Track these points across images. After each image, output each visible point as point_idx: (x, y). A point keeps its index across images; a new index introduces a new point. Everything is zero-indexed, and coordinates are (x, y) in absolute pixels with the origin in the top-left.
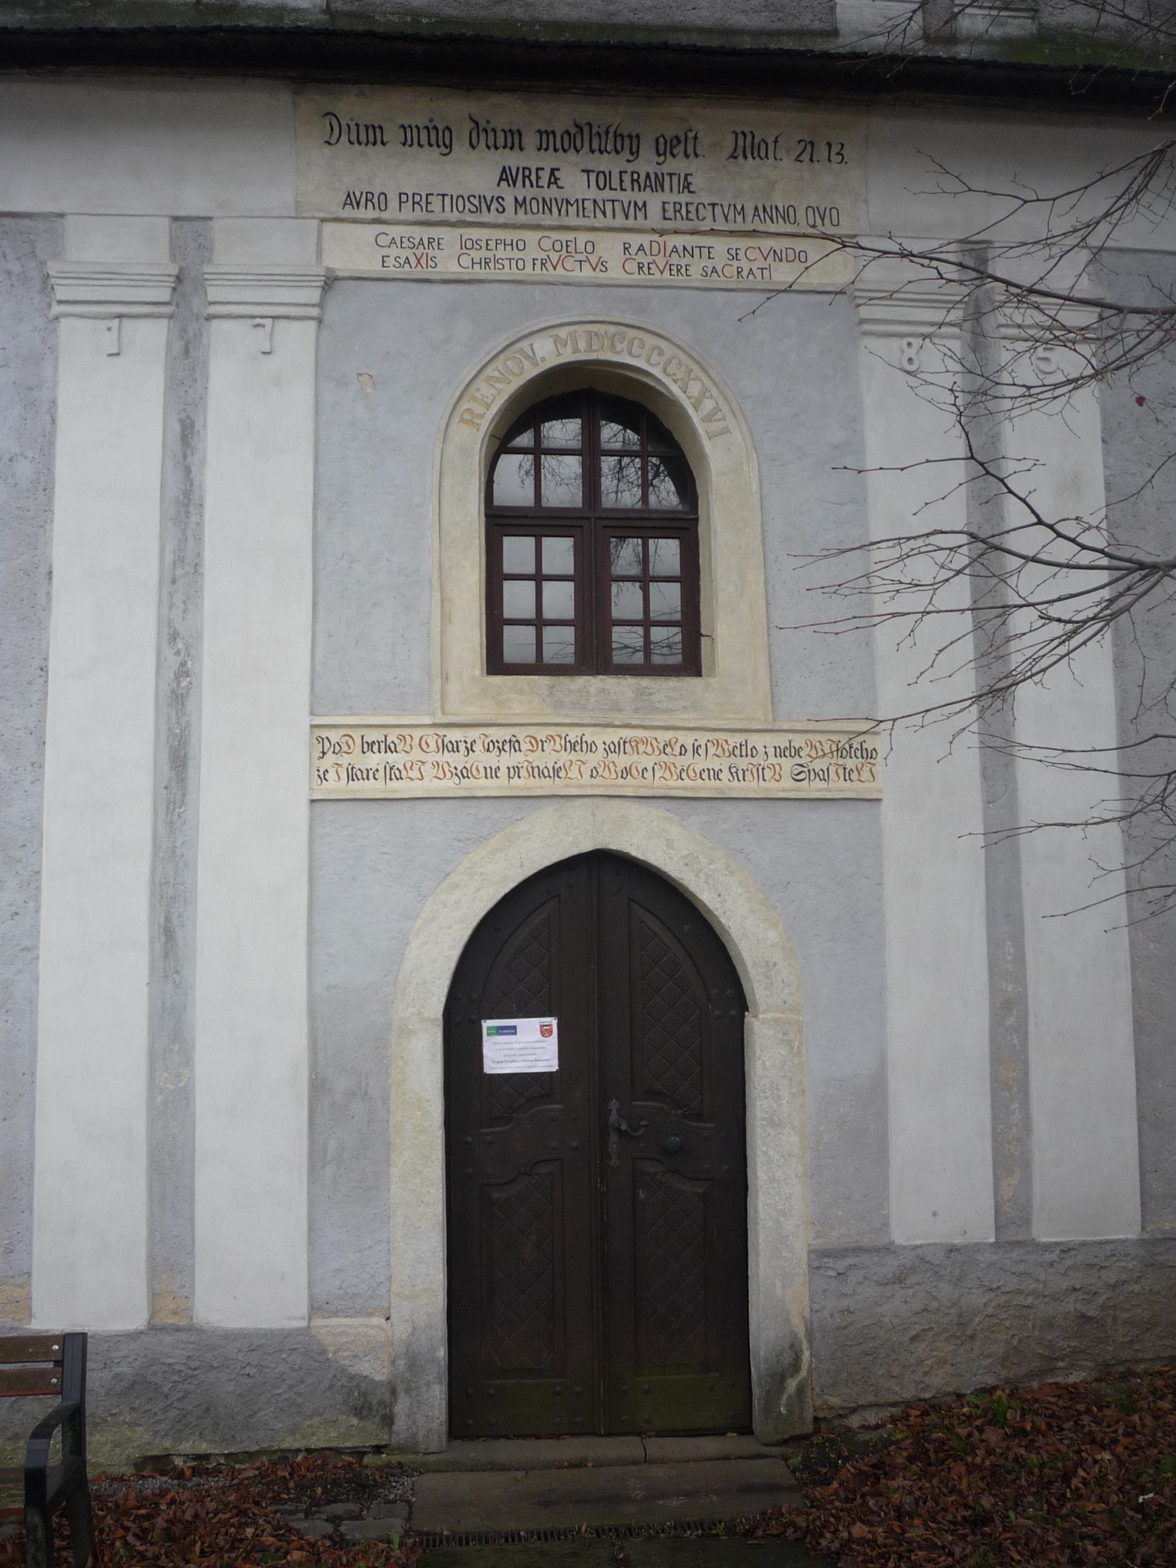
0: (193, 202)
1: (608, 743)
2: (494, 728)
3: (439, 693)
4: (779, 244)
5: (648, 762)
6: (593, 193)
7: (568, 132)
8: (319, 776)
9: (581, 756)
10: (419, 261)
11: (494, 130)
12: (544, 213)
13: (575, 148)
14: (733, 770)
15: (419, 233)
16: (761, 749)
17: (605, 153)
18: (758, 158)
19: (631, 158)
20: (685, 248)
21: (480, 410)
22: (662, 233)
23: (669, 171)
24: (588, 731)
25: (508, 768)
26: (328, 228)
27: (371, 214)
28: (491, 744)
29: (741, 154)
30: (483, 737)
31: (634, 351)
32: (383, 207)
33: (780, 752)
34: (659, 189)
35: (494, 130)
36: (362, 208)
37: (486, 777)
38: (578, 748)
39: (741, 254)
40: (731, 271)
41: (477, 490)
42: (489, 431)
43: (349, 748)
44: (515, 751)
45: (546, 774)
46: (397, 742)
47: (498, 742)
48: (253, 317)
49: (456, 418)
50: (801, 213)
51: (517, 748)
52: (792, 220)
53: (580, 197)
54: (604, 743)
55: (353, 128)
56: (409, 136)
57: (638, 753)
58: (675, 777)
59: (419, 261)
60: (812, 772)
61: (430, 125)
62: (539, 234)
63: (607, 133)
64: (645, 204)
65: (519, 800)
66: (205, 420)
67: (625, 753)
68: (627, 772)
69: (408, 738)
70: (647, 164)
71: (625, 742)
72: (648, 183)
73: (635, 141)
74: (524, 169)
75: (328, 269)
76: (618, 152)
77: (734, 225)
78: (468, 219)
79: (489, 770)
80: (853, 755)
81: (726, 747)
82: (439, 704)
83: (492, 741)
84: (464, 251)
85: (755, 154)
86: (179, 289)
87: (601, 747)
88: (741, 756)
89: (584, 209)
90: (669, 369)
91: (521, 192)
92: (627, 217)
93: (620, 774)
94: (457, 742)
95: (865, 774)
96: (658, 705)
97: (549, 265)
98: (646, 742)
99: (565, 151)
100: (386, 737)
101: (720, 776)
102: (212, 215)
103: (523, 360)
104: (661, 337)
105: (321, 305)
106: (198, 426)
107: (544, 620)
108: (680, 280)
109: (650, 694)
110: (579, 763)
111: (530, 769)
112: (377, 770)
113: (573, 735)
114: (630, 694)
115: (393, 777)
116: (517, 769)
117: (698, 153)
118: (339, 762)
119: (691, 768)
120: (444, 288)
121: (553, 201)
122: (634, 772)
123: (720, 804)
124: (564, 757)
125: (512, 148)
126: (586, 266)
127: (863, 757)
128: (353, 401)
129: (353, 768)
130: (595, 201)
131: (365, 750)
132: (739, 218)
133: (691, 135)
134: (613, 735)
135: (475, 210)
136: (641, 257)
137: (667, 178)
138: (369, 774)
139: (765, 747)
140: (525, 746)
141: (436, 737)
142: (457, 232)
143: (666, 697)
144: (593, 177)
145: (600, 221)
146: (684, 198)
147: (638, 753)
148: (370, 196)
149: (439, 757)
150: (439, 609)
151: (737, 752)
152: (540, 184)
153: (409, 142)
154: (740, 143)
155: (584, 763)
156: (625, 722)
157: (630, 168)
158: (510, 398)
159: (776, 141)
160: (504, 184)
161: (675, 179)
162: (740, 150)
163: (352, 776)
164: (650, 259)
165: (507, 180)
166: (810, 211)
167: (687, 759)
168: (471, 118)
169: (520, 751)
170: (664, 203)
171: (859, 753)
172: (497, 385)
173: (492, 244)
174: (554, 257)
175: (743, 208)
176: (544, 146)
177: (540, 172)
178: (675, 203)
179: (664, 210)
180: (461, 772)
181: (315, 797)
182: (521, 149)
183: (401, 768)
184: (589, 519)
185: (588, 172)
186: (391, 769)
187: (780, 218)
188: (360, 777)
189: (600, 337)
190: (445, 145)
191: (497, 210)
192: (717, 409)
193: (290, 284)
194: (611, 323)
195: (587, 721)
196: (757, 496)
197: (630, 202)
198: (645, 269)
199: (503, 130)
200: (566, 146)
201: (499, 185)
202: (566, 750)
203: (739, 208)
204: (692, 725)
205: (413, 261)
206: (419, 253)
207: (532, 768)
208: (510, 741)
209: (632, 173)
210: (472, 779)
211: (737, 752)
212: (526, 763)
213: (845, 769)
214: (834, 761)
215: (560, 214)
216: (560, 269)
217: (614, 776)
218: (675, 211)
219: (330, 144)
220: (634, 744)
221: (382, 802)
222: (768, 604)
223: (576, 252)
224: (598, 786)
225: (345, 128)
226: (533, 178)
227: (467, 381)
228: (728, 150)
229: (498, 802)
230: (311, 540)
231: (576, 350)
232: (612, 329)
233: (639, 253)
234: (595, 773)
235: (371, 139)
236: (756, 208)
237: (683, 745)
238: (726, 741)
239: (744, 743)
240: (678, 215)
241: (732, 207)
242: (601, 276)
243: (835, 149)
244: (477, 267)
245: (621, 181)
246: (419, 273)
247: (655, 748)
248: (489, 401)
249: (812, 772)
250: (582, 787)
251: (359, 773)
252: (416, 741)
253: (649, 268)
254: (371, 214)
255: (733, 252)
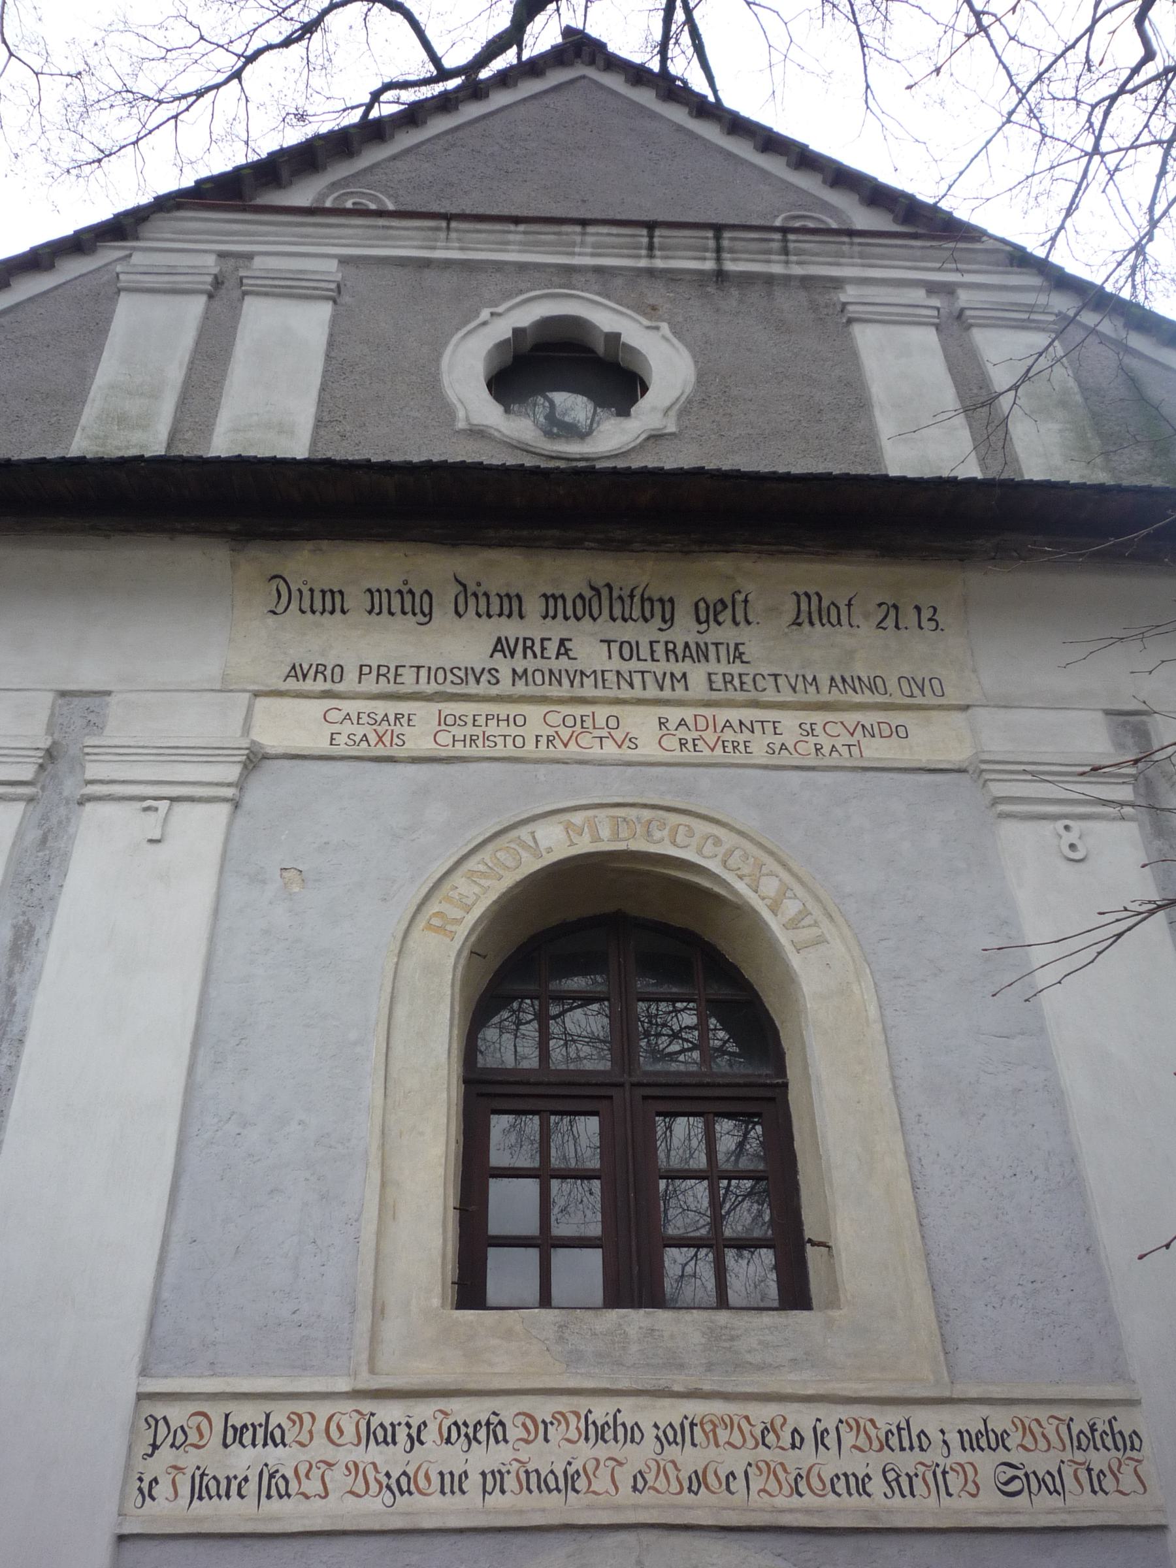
0: (88, 676)
1: (662, 1427)
2: (462, 1399)
3: (367, 1336)
4: (869, 718)
5: (735, 1461)
6: (616, 663)
7: (581, 596)
8: (140, 1490)
9: (613, 1449)
10: (380, 739)
11: (486, 595)
12: (550, 684)
13: (591, 615)
14: (891, 1476)
15: (381, 708)
16: (936, 1437)
17: (630, 622)
18: (828, 625)
19: (664, 626)
20: (741, 723)
21: (456, 913)
22: (708, 704)
23: (714, 641)
24: (625, 1403)
25: (483, 1474)
26: (262, 702)
27: (320, 685)
28: (454, 1429)
29: (807, 621)
30: (440, 1416)
31: (678, 840)
32: (337, 678)
33: (971, 1441)
34: (702, 658)
35: (486, 595)
36: (309, 680)
37: (443, 1492)
38: (609, 1435)
39: (818, 729)
40: (807, 747)
41: (447, 1022)
42: (469, 944)
43: (201, 1436)
44: (497, 1442)
45: (552, 1485)
46: (286, 1425)
47: (466, 1424)
48: (145, 799)
49: (421, 923)
50: (892, 684)
51: (500, 1437)
52: (882, 690)
53: (599, 668)
54: (656, 1426)
55: (307, 594)
56: (376, 601)
57: (717, 1445)
58: (786, 1490)
59: (380, 739)
60: (1032, 1477)
61: (405, 589)
62: (544, 709)
63: (632, 596)
64: (684, 675)
65: (501, 1537)
66: (51, 925)
67: (694, 1445)
68: (698, 1481)
69: (307, 1419)
70: (684, 631)
71: (692, 1425)
72: (687, 654)
73: (668, 607)
74: (525, 639)
75: (253, 742)
76: (646, 620)
77: (805, 695)
78: (449, 690)
79: (447, 1478)
80: (1099, 1445)
81: (872, 1432)
82: (364, 1356)
83: (455, 1424)
84: (443, 727)
85: (825, 621)
86: (50, 767)
87: (650, 1433)
88: (902, 1449)
89: (604, 680)
90: (730, 862)
91: (519, 664)
92: (661, 688)
93: (686, 1485)
94: (392, 1425)
95: (1128, 1480)
96: (749, 1358)
97: (557, 742)
98: (730, 1424)
99: (578, 619)
100: (268, 1416)
101: (869, 1488)
102: (108, 689)
103: (520, 850)
104: (717, 822)
105: (240, 785)
106: (39, 933)
107: (552, 1238)
108: (738, 758)
109: (732, 1339)
110: (611, 1463)
111: (523, 1476)
112: (246, 1479)
113: (601, 1410)
114: (697, 1338)
115: (274, 1492)
116: (499, 1475)
117: (750, 618)
118: (180, 1464)
119: (815, 1471)
120: (412, 769)
121: (563, 673)
122: (711, 1479)
123: (873, 1542)
124: (585, 1452)
125: (509, 616)
126: (608, 743)
127: (1118, 1449)
128: (271, 903)
129: (203, 1475)
130: (618, 673)
131: (229, 1440)
132: (812, 689)
133: (740, 598)
134: (671, 1412)
135: (460, 681)
136: (682, 732)
137: (712, 649)
138: (232, 1487)
139: (942, 1432)
140: (514, 1433)
141: (356, 1416)
142: (434, 707)
143: (760, 1343)
144: (615, 648)
145: (626, 692)
146: (736, 668)
147: (717, 1445)
148: (321, 668)
149: (358, 1454)
150: (377, 1197)
151: (894, 1441)
152: (545, 655)
153: (377, 610)
154: (804, 606)
155: (620, 1464)
156: (692, 1386)
157: (663, 637)
158: (499, 898)
159: (849, 605)
160: (498, 655)
161: (723, 649)
162: (804, 617)
163: (199, 1491)
164: (696, 735)
165: (503, 651)
166: (904, 682)
167: (806, 1457)
168: (457, 580)
169: (505, 1441)
170: (709, 674)
171: (1109, 1441)
172: (482, 882)
173: (481, 720)
174: (565, 733)
175: (814, 679)
176: (551, 613)
177: (546, 643)
178: (724, 674)
179: (711, 681)
180: (398, 1481)
181: (126, 1530)
182: (521, 617)
183: (290, 1474)
184: (621, 1085)
185: (609, 642)
186: (272, 1476)
187: (865, 689)
188: (213, 1492)
189: (631, 823)
190: (422, 612)
191: (489, 682)
192: (804, 913)
193: (201, 759)
194: (645, 806)
195: (624, 1384)
196: (878, 1027)
197: (665, 674)
198: (690, 745)
199: (498, 595)
200: (580, 613)
201: (491, 656)
202: (587, 1439)
203: (810, 679)
204: (810, 1392)
205: (373, 738)
206: (381, 730)
207: (527, 1472)
208: (488, 1424)
209: (667, 643)
210: (416, 1495)
211: (894, 1441)
212: (516, 1465)
213: (1089, 1470)
214: (1067, 1456)
215: (572, 686)
216: (572, 746)
217: (675, 1487)
218: (725, 682)
219: (275, 613)
220: (708, 1427)
221: (248, 1542)
222: (915, 1188)
223: (594, 728)
224: (646, 1507)
225: (295, 594)
226: (537, 649)
227: (438, 876)
228: (790, 616)
229: (465, 1542)
230: (182, 1090)
231: (597, 839)
232: (647, 814)
233: (680, 728)
234: (640, 1485)
235: (329, 606)
236: (832, 679)
237: (795, 1430)
238: (872, 1421)
239: (903, 1425)
240: (729, 686)
241: (800, 678)
242: (628, 754)
243: (926, 614)
244: (459, 745)
245: (652, 652)
246: (380, 751)
247: (748, 1436)
248: (469, 902)
249: (1032, 1477)
250: (618, 1508)
251: (212, 1484)
252: (321, 1424)
253: (695, 745)
254: (320, 685)
255: (808, 727)
